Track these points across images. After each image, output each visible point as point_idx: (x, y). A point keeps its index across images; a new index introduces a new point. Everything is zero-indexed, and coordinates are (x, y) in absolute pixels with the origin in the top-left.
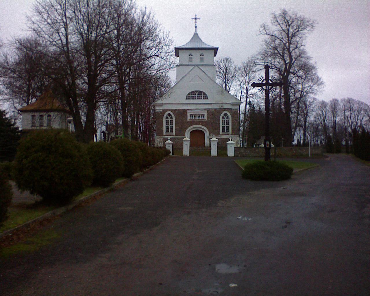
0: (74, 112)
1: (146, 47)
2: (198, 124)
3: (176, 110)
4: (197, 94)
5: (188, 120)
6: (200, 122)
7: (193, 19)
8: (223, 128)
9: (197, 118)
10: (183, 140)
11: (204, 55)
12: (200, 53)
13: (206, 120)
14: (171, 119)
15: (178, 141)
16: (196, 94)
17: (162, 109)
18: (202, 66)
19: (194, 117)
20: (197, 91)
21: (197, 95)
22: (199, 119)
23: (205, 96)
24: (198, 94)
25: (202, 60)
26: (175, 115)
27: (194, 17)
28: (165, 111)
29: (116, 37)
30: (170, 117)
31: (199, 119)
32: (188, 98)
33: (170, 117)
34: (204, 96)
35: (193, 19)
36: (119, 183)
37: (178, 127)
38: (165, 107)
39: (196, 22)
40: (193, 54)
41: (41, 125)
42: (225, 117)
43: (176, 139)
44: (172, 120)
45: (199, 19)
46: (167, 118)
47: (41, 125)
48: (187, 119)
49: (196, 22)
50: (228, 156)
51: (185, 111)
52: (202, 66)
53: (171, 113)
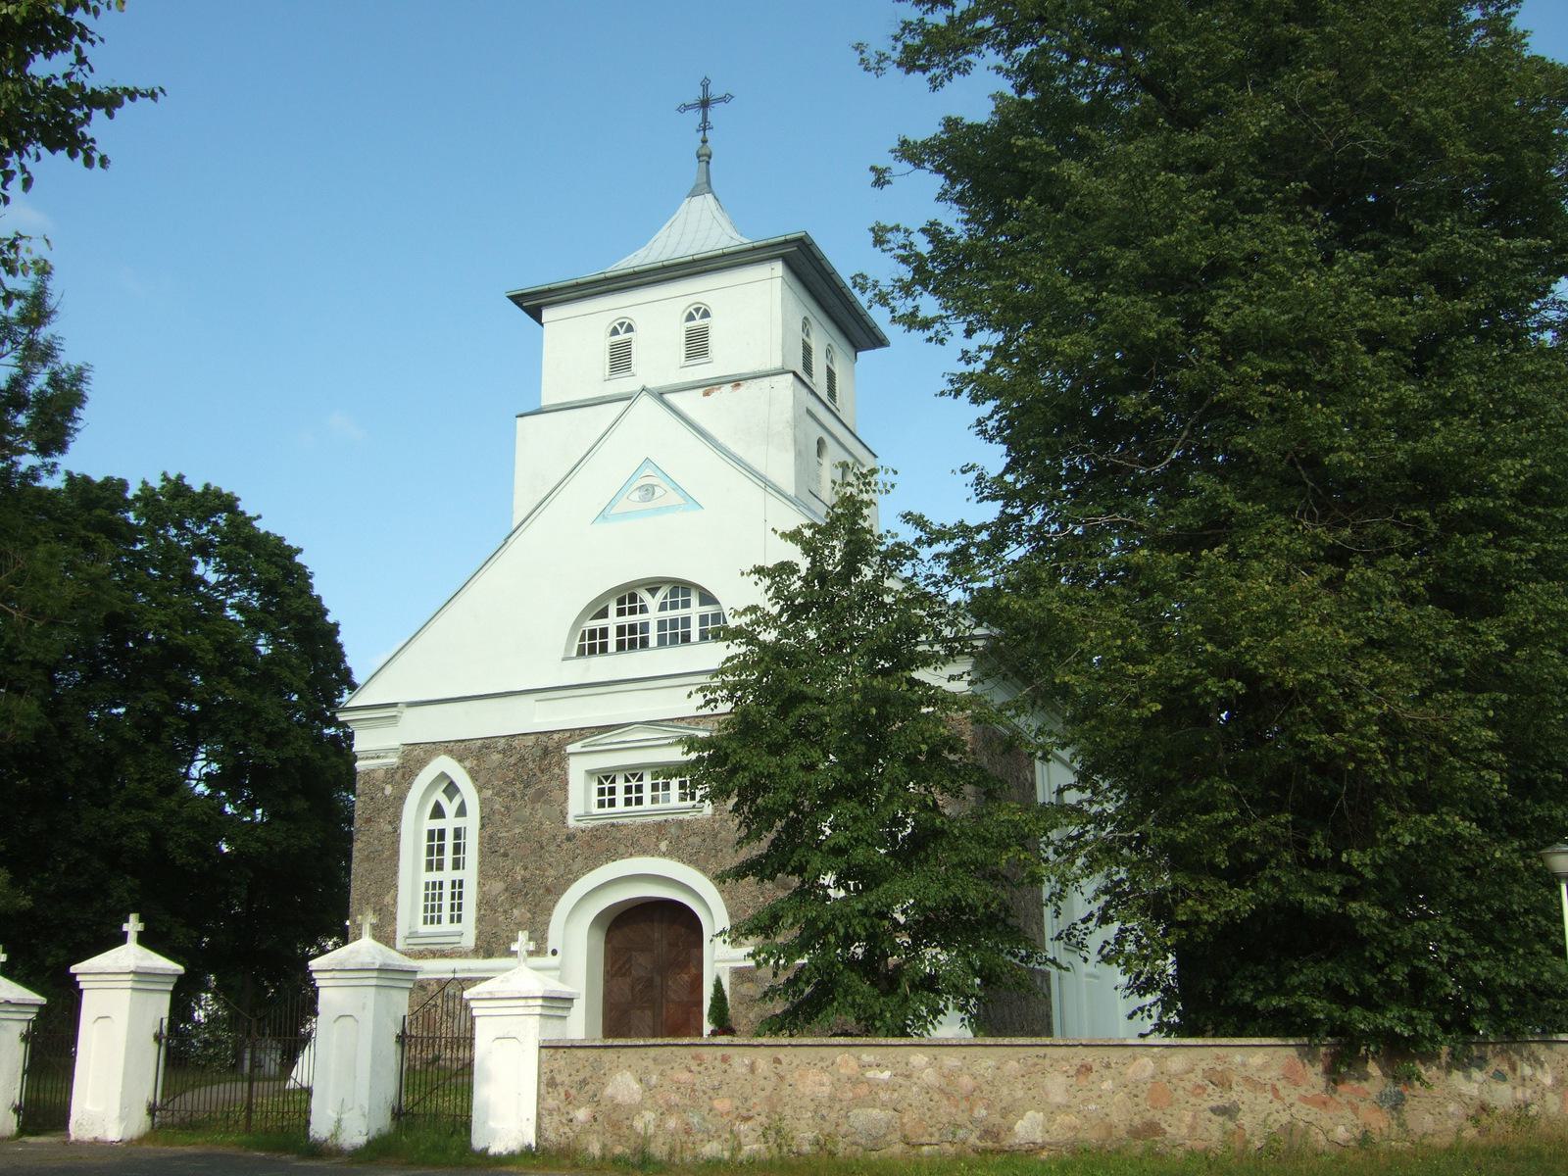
1: (1050, 540)
2: (645, 852)
3: (487, 744)
5: (571, 822)
6: (661, 828)
9: (647, 804)
10: (467, 995)
11: (712, 313)
12: (683, 306)
16: (644, 609)
17: (396, 743)
18: (709, 386)
19: (628, 790)
20: (653, 586)
21: (653, 616)
22: (660, 805)
24: (663, 607)
25: (697, 344)
26: (480, 790)
27: (695, 95)
28: (414, 759)
31: (660, 805)
32: (593, 644)
33: (457, 801)
35: (687, 107)
36: (791, 1035)
37: (498, 886)
39: (705, 126)
40: (636, 316)
45: (725, 99)
48: (564, 815)
49: (705, 126)
52: (709, 386)
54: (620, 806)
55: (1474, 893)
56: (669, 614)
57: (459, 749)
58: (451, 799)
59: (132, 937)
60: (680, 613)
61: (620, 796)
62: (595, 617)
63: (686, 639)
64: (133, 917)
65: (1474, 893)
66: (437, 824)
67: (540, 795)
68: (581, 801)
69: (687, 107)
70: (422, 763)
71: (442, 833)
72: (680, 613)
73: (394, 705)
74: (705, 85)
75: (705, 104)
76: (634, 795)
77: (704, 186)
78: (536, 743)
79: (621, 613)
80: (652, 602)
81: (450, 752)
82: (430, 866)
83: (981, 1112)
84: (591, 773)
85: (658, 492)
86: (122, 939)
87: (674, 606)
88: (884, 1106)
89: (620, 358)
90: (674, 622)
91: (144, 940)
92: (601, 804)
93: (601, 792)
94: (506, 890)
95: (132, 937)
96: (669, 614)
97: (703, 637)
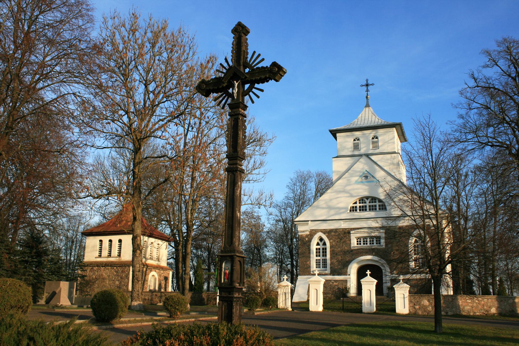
0: (177, 239)
4: (368, 201)
7: (362, 86)
8: (318, 262)
12: (372, 136)
13: (384, 247)
14: (324, 247)
15: (335, 284)
16: (365, 203)
19: (364, 241)
20: (367, 198)
21: (368, 204)
23: (382, 205)
24: (370, 202)
25: (375, 145)
26: (329, 240)
27: (365, 83)
28: (313, 233)
29: (483, 84)
30: (323, 242)
33: (323, 242)
34: (379, 206)
35: (363, 86)
38: (312, 226)
39: (367, 91)
41: (110, 255)
42: (321, 244)
43: (333, 281)
44: (326, 249)
45: (372, 85)
46: (318, 244)
47: (110, 255)
49: (367, 91)
50: (310, 309)
51: (347, 232)
53: (324, 237)
54: (362, 244)
55: (5, 238)
56: (371, 204)
57: (324, 232)
58: (321, 242)
59: (368, 275)
60: (374, 204)
61: (362, 243)
62: (354, 204)
63: (366, 210)
64: (368, 271)
65: (5, 238)
66: (318, 247)
67: (344, 242)
68: (354, 243)
69: (363, 86)
70: (315, 234)
71: (319, 249)
72: (374, 204)
73: (308, 221)
74: (367, 80)
75: (367, 85)
76: (359, 243)
77: (367, 106)
78: (343, 230)
79: (360, 203)
80: (368, 201)
81: (322, 232)
82: (317, 256)
83: (485, 308)
84: (320, 236)
85: (369, 178)
86: (367, 275)
87: (372, 202)
88: (470, 306)
89: (356, 147)
90: (373, 206)
91: (371, 275)
92: (358, 244)
93: (357, 241)
94: (337, 261)
95: (368, 275)
96: (371, 204)
97: (370, 210)
